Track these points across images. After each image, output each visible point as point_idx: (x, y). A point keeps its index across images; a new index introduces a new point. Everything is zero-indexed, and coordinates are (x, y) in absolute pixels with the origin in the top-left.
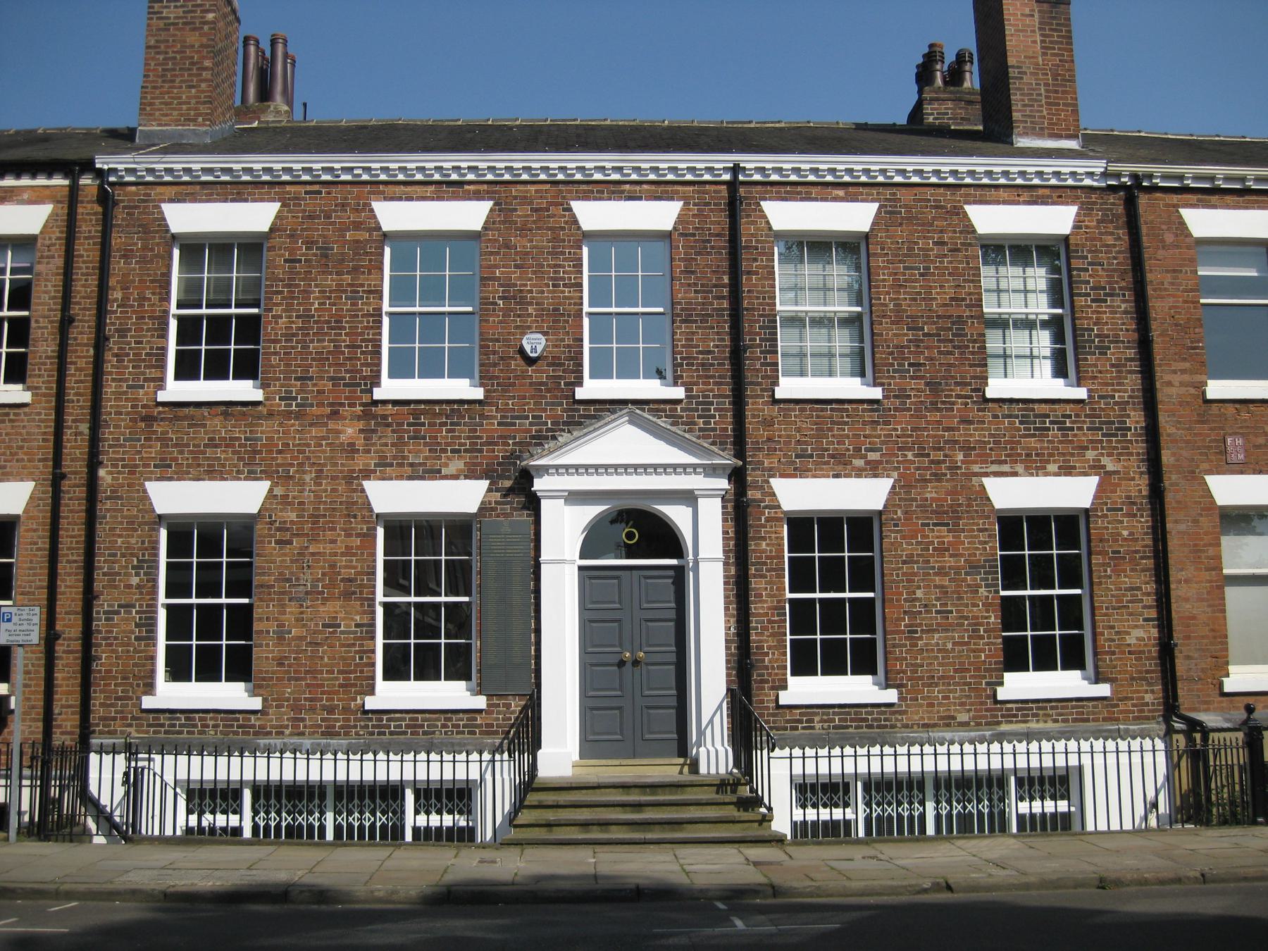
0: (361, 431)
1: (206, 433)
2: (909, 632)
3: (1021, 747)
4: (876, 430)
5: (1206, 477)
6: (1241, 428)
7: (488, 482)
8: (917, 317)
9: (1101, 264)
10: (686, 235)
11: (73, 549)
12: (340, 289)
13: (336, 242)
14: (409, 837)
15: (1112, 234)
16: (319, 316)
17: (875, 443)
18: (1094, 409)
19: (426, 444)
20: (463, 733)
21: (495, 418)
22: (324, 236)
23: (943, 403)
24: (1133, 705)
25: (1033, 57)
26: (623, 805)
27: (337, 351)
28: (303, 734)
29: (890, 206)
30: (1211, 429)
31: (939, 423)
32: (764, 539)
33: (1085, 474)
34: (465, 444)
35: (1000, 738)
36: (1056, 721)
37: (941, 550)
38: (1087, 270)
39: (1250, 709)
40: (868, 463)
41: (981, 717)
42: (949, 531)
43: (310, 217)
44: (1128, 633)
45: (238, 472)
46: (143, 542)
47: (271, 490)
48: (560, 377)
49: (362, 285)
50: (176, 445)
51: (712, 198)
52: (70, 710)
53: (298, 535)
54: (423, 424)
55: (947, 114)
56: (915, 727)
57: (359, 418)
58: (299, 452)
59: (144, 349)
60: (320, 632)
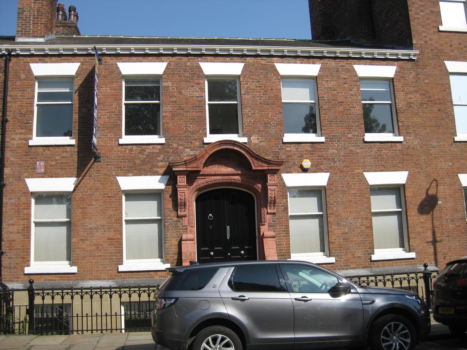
6: (45, 157)
25: (29, 4)
30: (30, 158)
39: (31, 282)
55: (60, 32)
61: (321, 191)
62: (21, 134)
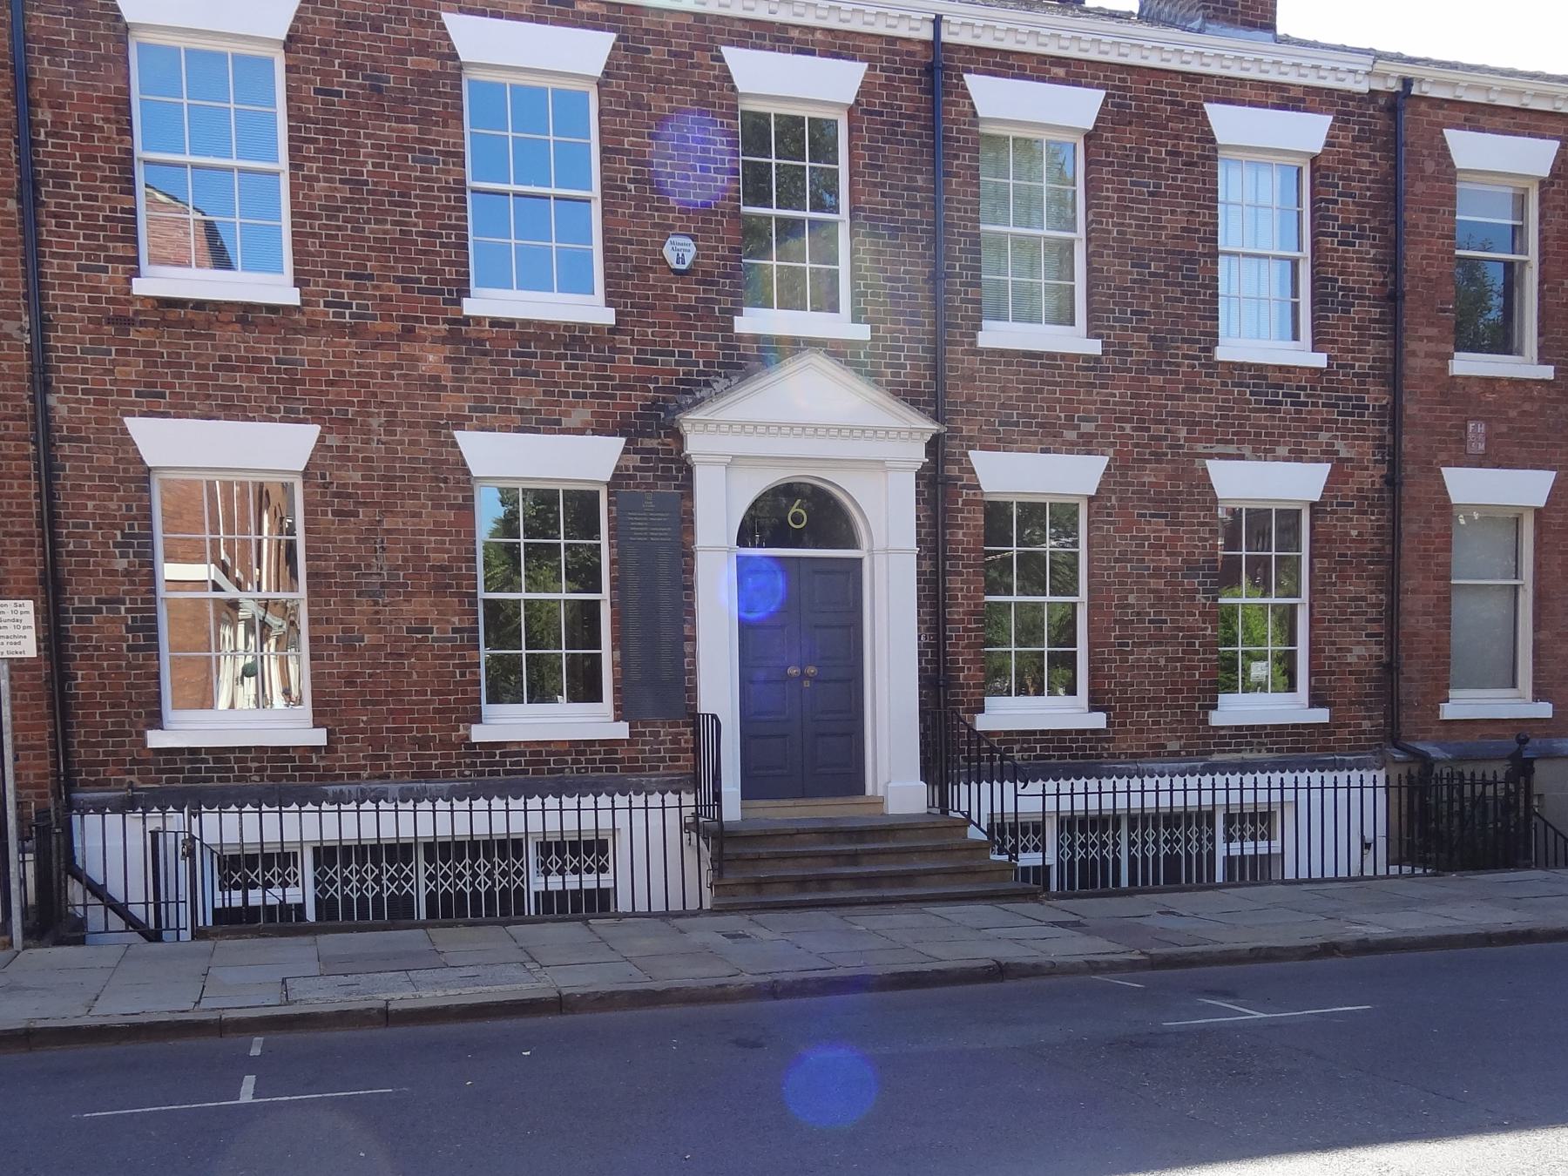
0: (447, 360)
1: (215, 348)
2: (1120, 645)
3: (1234, 780)
4: (1091, 395)
5: (1442, 469)
7: (623, 440)
8: (1144, 250)
9: (1352, 196)
10: (871, 113)
11: (14, 515)
12: (402, 145)
13: (392, 71)
14: (530, 907)
15: (1367, 156)
16: (375, 184)
17: (1090, 411)
18: (1331, 381)
19: (538, 384)
20: (600, 770)
21: (630, 352)
22: (374, 59)
23: (1168, 364)
24: (1350, 733)
26: (835, 856)
27: (405, 239)
28: (387, 776)
29: (1119, 97)
31: (1162, 389)
32: (960, 527)
33: (1317, 461)
34: (591, 387)
35: (1212, 769)
36: (1269, 750)
37: (1157, 548)
38: (1336, 202)
40: (1081, 436)
41: (1192, 746)
42: (1167, 524)
43: (348, 25)
44: (1350, 651)
45: (270, 410)
46: (129, 508)
47: (321, 439)
48: (713, 301)
49: (436, 143)
50: (169, 365)
51: (902, 61)
52: (31, 753)
53: (365, 504)
54: (534, 355)
56: (1123, 757)
57: (444, 341)
58: (361, 385)
59: (101, 209)
60: (404, 639)
61: (1517, 521)
62: (1430, 339)
